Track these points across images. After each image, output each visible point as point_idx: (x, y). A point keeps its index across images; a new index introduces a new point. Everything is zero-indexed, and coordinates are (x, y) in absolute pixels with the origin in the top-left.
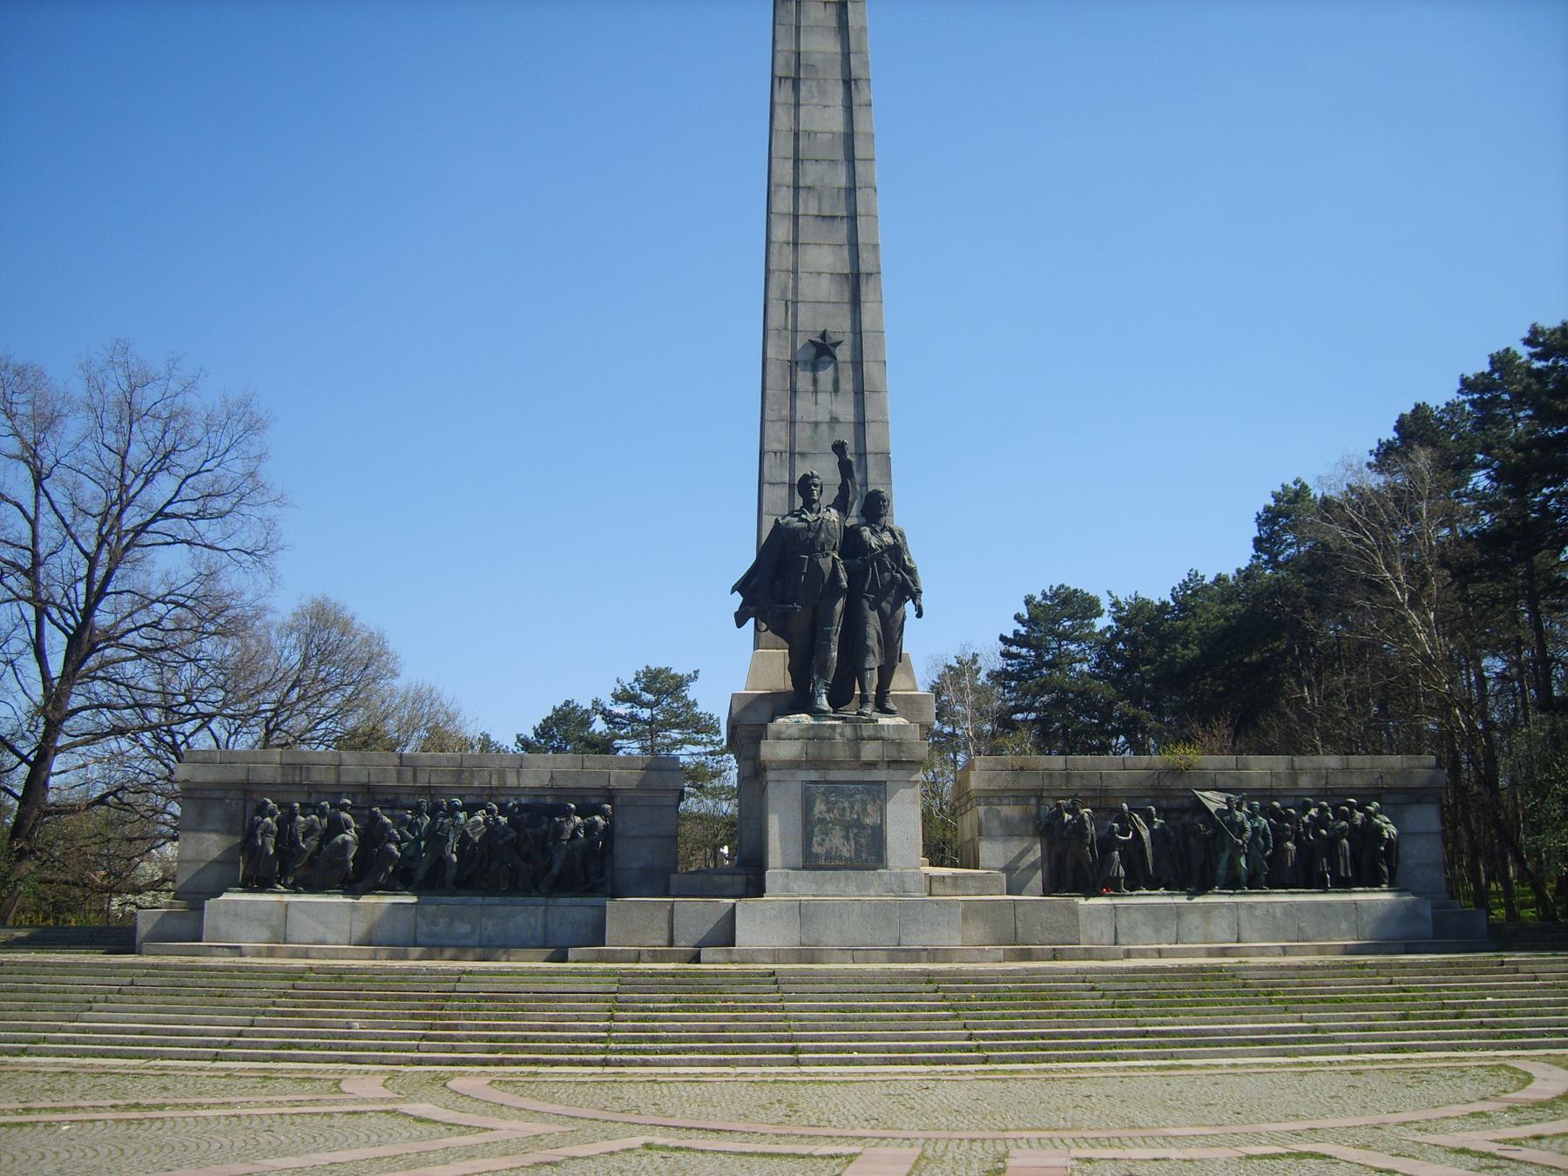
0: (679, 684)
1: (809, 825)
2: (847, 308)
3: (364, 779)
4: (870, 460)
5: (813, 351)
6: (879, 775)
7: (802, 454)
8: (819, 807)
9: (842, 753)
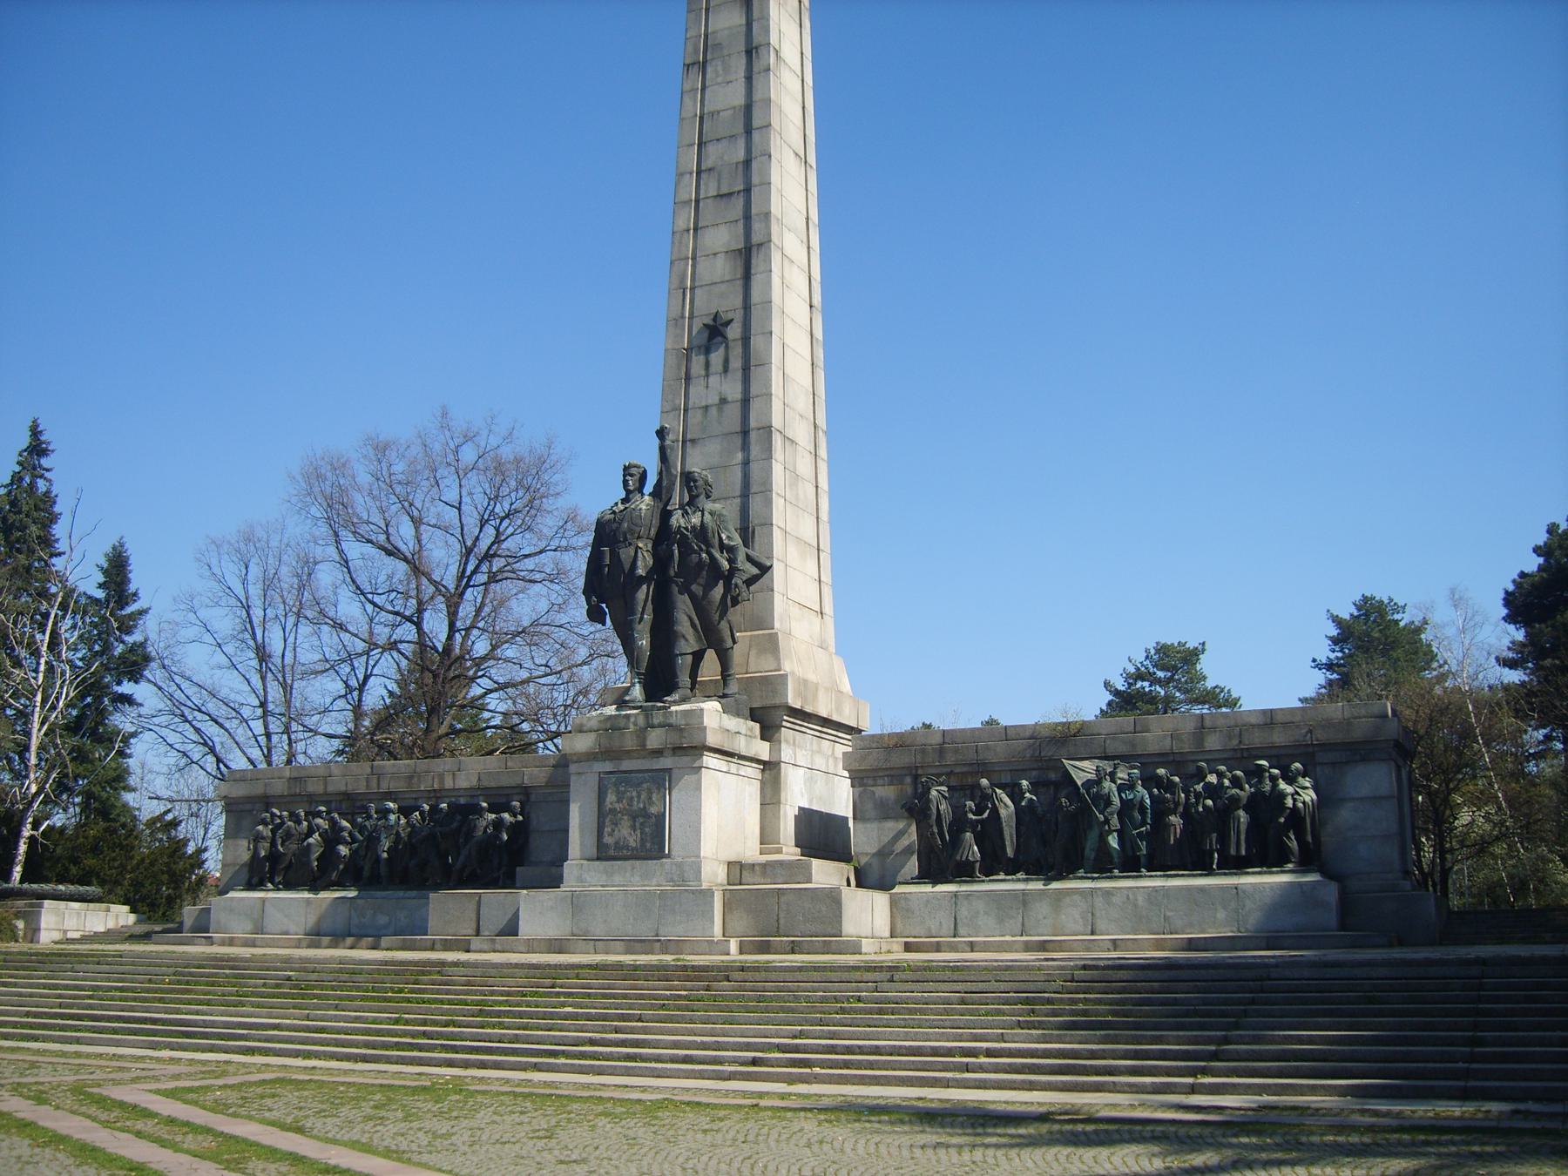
0: (1190, 657)
1: (603, 816)
2: (739, 283)
3: (343, 789)
4: (753, 435)
5: (706, 335)
6: (666, 762)
7: (693, 441)
8: (611, 798)
9: (630, 743)
